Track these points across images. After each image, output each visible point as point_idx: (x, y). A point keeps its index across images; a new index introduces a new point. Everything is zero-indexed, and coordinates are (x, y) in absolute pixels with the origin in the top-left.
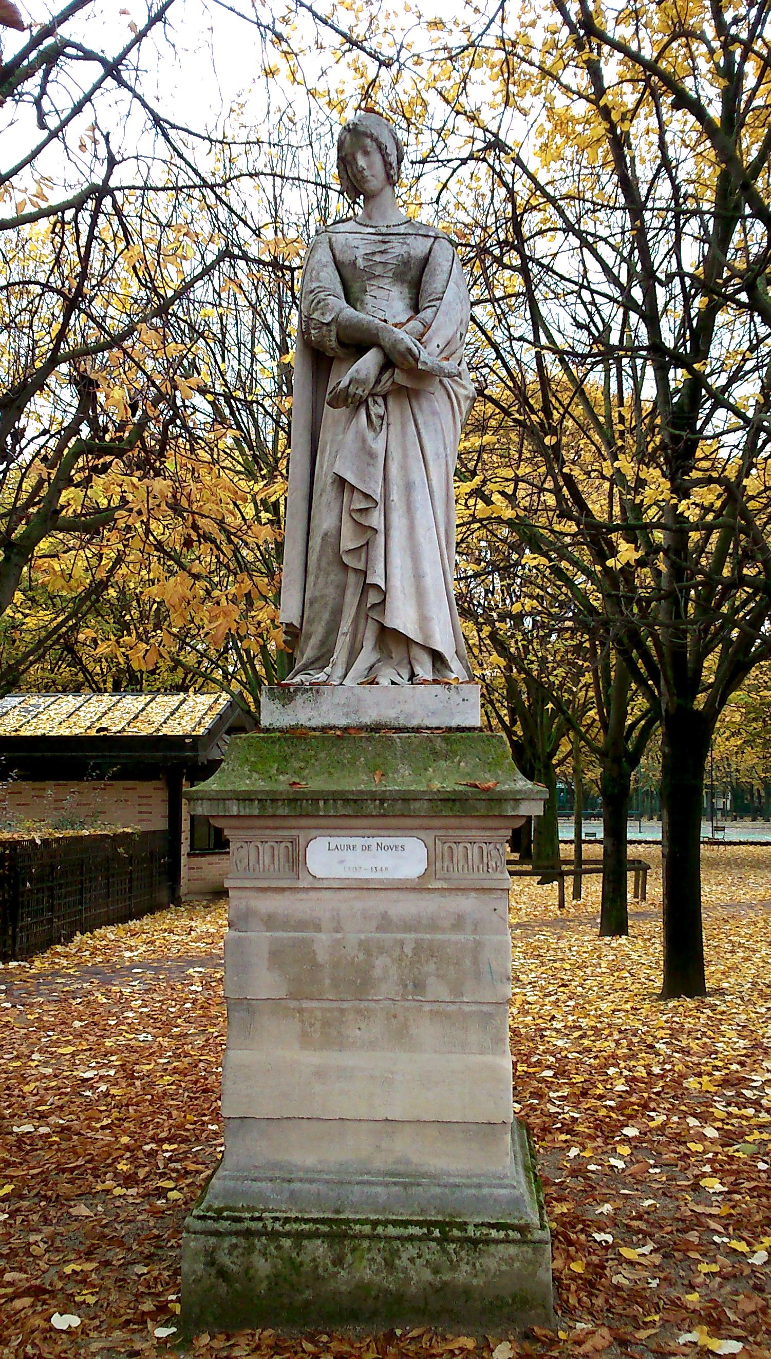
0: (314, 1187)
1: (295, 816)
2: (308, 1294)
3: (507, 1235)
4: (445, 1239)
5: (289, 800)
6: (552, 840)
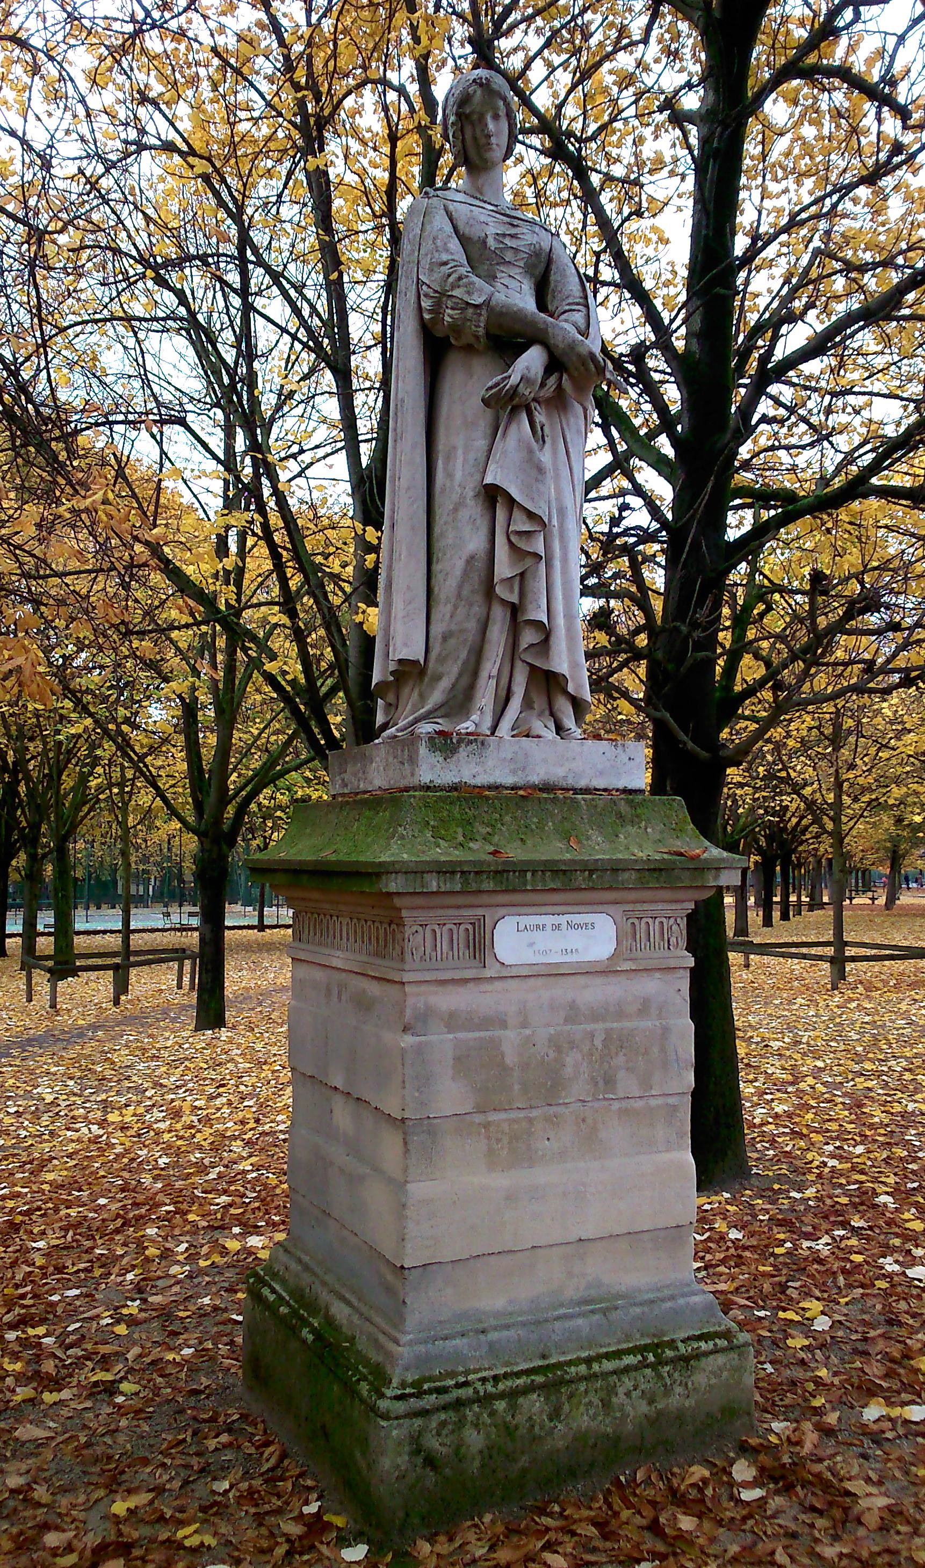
0: (511, 1333)
1: (503, 891)
2: (524, 1461)
3: (715, 1345)
4: (660, 1362)
5: (496, 872)
6: (67, 932)
